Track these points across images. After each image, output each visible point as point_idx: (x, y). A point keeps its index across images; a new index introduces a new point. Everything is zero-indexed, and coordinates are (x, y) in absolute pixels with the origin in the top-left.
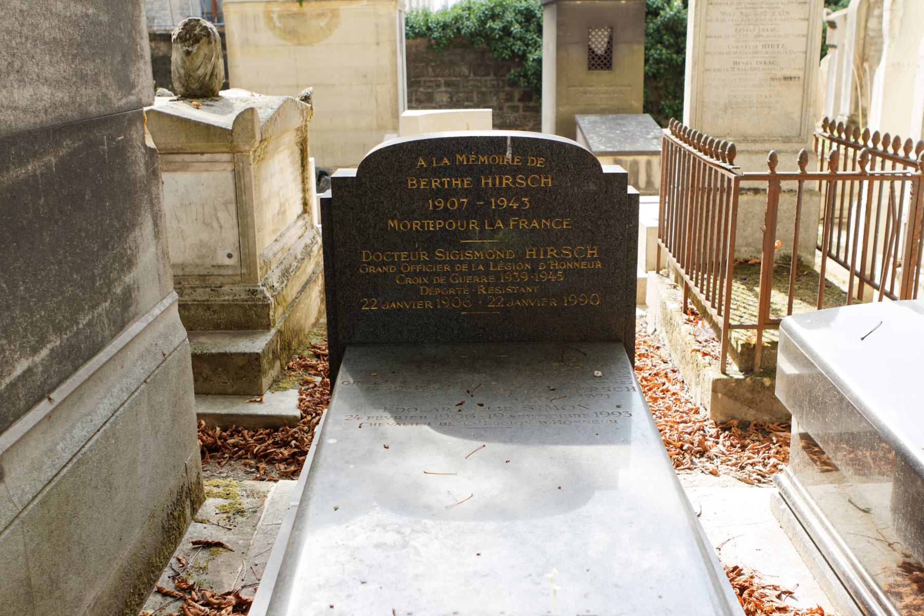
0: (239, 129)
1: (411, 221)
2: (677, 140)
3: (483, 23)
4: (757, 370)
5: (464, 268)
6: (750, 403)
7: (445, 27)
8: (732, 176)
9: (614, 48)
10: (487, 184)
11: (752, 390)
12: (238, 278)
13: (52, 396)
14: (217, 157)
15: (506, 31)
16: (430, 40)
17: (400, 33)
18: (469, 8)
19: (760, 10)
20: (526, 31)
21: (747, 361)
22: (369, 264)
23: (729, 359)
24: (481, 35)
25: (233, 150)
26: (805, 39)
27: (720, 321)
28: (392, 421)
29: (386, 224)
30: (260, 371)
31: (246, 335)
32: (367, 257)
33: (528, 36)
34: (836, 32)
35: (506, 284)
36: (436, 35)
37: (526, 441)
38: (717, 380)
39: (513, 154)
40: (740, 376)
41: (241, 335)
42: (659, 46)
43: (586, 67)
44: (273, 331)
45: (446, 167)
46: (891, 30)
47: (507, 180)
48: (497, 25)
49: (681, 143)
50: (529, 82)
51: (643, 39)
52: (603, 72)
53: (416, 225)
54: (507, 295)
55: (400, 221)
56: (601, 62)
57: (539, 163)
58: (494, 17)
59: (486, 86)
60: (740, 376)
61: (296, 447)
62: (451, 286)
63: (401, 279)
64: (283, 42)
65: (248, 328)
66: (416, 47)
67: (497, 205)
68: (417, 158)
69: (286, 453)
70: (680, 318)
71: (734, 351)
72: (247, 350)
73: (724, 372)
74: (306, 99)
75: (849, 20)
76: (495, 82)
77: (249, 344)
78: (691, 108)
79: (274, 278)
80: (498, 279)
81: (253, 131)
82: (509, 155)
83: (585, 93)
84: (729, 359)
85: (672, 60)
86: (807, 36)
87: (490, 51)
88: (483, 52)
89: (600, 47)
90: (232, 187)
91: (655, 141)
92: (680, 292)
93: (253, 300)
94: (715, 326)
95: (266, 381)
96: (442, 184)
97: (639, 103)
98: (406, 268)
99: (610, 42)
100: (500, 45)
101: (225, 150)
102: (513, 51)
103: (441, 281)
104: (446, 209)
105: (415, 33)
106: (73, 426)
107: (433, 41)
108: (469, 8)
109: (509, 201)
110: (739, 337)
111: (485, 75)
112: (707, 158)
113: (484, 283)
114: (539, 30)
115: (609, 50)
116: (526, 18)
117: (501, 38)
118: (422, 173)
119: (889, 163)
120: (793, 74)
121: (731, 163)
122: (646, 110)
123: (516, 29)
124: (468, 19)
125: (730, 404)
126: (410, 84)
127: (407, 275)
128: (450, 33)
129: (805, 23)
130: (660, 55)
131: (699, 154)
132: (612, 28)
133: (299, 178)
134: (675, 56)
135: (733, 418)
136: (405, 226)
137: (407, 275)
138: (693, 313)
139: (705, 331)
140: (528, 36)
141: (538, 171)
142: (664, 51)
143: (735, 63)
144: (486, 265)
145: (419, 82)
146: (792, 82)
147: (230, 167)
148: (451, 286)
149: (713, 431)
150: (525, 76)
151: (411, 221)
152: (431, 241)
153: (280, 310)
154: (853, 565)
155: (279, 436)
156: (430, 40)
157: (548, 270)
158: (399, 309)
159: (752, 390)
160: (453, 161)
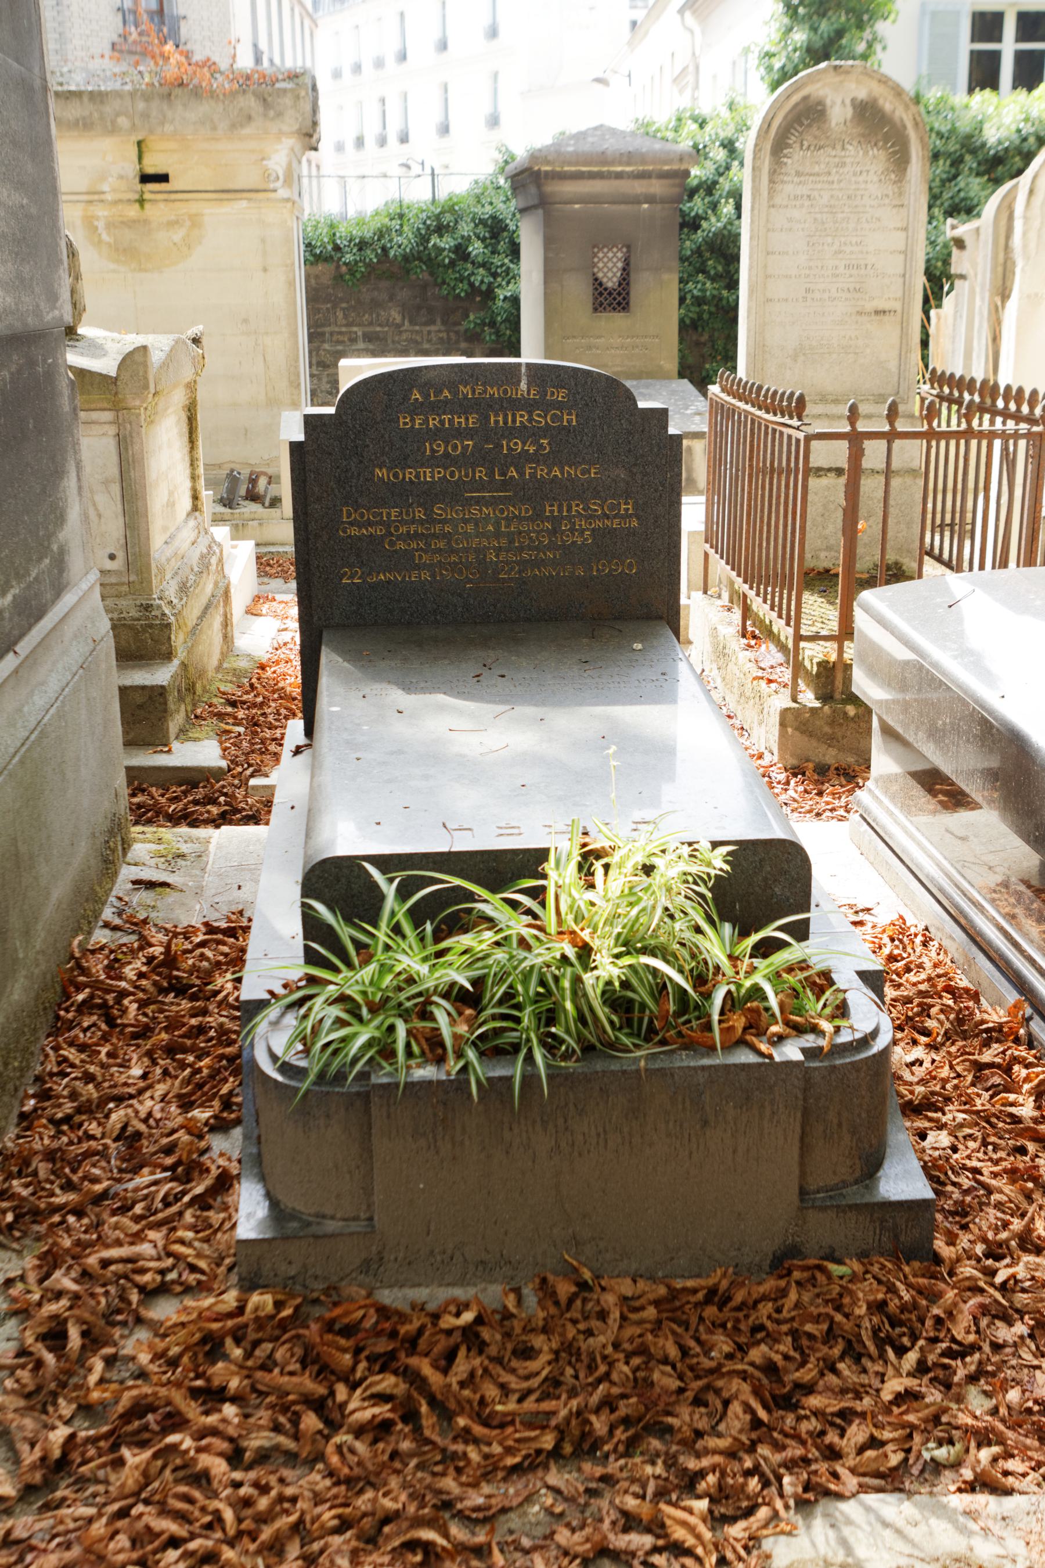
0: (125, 376)
1: (403, 469)
2: (729, 399)
3: (424, 239)
4: (837, 696)
5: (470, 528)
6: (830, 740)
7: (362, 245)
8: (801, 435)
9: (633, 276)
10: (497, 422)
11: (832, 723)
12: (125, 588)
13: (17, 649)
14: (95, 415)
15: (461, 252)
16: (338, 267)
17: (297, 254)
18: (401, 216)
19: (840, 216)
20: (493, 253)
21: (824, 686)
22: (351, 524)
23: (802, 685)
24: (420, 259)
25: (117, 406)
26: (902, 257)
27: (786, 633)
28: (400, 692)
29: (372, 473)
30: (165, 711)
31: (141, 667)
32: (349, 515)
33: (496, 260)
34: (966, 254)
35: (521, 549)
36: (348, 258)
37: (560, 704)
38: (787, 710)
39: (529, 384)
40: (817, 704)
41: (133, 667)
42: (701, 277)
43: (590, 306)
44: (176, 662)
45: (446, 402)
46: (1025, 246)
47: (522, 418)
48: (446, 242)
49: (734, 401)
50: (497, 333)
51: (676, 264)
52: (616, 314)
53: (410, 474)
54: (523, 563)
55: (389, 469)
56: (613, 299)
57: (561, 395)
58: (441, 229)
59: (429, 341)
60: (817, 704)
61: (227, 804)
62: (453, 551)
63: (392, 544)
64: (112, 266)
65: (141, 658)
66: (317, 277)
67: (509, 449)
68: (410, 390)
69: (215, 810)
70: (737, 644)
71: (808, 673)
72: (147, 683)
73: (795, 700)
74: (196, 341)
75: (982, 237)
76: (444, 335)
77: (148, 676)
78: (748, 354)
79: (171, 591)
80: (511, 542)
81: (146, 378)
82: (523, 385)
83: (590, 348)
84: (802, 685)
85: (721, 299)
86: (905, 252)
87: (436, 284)
88: (424, 287)
89: (611, 279)
90: (115, 459)
91: (697, 418)
92: (737, 615)
93: (147, 618)
94: (783, 648)
95: (173, 726)
96: (442, 422)
97: (672, 365)
98: (397, 528)
99: (626, 270)
100: (451, 275)
101: (105, 405)
102: (471, 285)
103: (441, 545)
104: (446, 455)
105: (315, 255)
106: (31, 694)
107: (344, 269)
108: (401, 216)
109: (524, 444)
110: (814, 653)
111: (426, 324)
112: (770, 417)
113: (494, 548)
114: (515, 252)
115: (625, 281)
116: (491, 232)
117: (452, 263)
118: (416, 409)
119: (999, 420)
120: (887, 307)
121: (800, 419)
122: (681, 375)
123: (476, 248)
124: (399, 232)
125: (802, 741)
126: (312, 337)
127: (399, 538)
128: (371, 255)
129: (902, 235)
130: (702, 290)
131: (759, 413)
132: (628, 247)
133: (187, 459)
134: (725, 293)
135: (808, 760)
136: (396, 476)
137: (399, 538)
138: (754, 637)
139: (770, 655)
140: (496, 260)
141: (560, 406)
142: (708, 285)
143: (808, 291)
144: (497, 524)
145: (323, 334)
146: (886, 318)
147: (112, 430)
148: (453, 551)
149: (782, 777)
150: (493, 324)
151: (403, 469)
152: (429, 495)
153: (181, 637)
154: (938, 865)
155: (200, 793)
156: (338, 267)
157: (572, 530)
158: (389, 582)
159: (832, 723)
160: (455, 393)
